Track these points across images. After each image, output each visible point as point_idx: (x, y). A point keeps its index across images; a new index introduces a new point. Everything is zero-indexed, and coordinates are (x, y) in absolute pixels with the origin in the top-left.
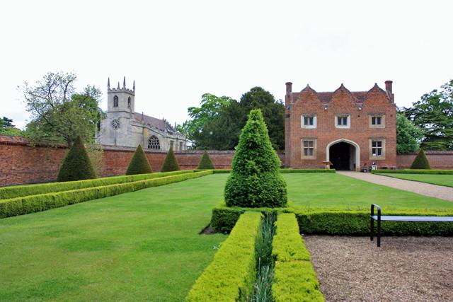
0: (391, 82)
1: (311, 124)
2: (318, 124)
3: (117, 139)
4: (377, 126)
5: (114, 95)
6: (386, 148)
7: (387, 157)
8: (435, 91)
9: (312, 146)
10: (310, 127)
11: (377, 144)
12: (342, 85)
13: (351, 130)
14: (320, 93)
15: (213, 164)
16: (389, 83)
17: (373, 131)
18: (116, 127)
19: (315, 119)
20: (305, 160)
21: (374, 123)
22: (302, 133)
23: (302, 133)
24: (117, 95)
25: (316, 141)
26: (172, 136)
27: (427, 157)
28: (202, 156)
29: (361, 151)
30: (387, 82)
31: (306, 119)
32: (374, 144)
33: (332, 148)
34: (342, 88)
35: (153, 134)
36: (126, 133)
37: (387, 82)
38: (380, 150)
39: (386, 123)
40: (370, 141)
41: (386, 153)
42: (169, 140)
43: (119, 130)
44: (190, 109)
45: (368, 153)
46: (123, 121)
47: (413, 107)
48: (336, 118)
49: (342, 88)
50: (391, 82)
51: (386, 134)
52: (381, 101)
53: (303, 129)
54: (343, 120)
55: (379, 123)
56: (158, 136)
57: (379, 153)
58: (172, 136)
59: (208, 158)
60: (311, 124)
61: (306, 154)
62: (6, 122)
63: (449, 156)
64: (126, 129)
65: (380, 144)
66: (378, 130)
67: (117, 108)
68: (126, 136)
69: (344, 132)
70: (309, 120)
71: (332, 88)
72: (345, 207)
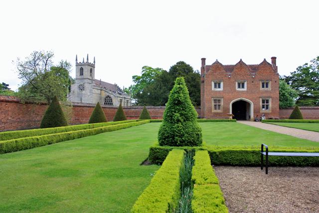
0: (275, 58)
1: (219, 87)
2: (224, 87)
3: (82, 98)
4: (265, 89)
5: (80, 67)
6: (272, 105)
7: (272, 111)
8: (306, 64)
9: (220, 103)
10: (218, 89)
11: (265, 101)
12: (241, 60)
13: (247, 91)
14: (225, 66)
15: (150, 116)
16: (274, 59)
17: (263, 92)
18: (81, 90)
19: (222, 84)
20: (215, 113)
21: (263, 87)
22: (212, 94)
23: (212, 94)
24: (83, 67)
25: (222, 99)
26: (121, 96)
27: (301, 111)
28: (142, 110)
29: (254, 107)
30: (272, 58)
31: (215, 84)
32: (263, 102)
33: (234, 105)
34: (241, 62)
35: (108, 94)
36: (89, 94)
37: (272, 58)
38: (267, 106)
39: (272, 87)
40: (261, 100)
41: (272, 108)
42: (119, 99)
43: (84, 92)
44: (134, 77)
45: (259, 108)
46: (86, 85)
47: (291, 76)
48: (237, 83)
49: (241, 62)
50: (275, 58)
51: (272, 95)
52: (268, 71)
53: (214, 91)
54: (241, 85)
55: (267, 87)
56: (112, 96)
57: (267, 108)
58: (121, 96)
59: (147, 112)
60: (219, 87)
61: (215, 109)
62: (5, 86)
63: (316, 110)
64: (89, 91)
65: (267, 102)
66: (267, 92)
67: (82, 76)
68: (89, 96)
69: (242, 93)
70: (217, 85)
71: (234, 62)
72: (243, 146)
